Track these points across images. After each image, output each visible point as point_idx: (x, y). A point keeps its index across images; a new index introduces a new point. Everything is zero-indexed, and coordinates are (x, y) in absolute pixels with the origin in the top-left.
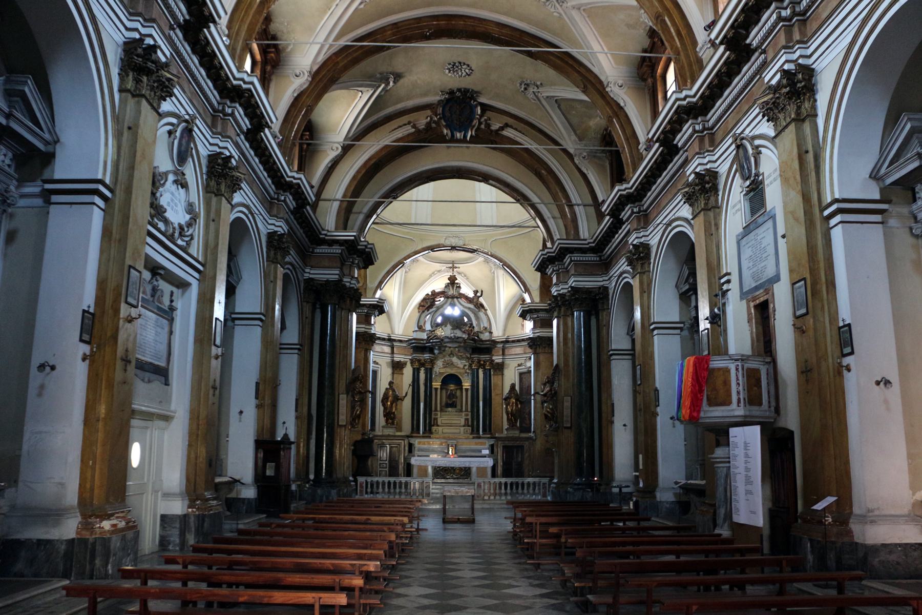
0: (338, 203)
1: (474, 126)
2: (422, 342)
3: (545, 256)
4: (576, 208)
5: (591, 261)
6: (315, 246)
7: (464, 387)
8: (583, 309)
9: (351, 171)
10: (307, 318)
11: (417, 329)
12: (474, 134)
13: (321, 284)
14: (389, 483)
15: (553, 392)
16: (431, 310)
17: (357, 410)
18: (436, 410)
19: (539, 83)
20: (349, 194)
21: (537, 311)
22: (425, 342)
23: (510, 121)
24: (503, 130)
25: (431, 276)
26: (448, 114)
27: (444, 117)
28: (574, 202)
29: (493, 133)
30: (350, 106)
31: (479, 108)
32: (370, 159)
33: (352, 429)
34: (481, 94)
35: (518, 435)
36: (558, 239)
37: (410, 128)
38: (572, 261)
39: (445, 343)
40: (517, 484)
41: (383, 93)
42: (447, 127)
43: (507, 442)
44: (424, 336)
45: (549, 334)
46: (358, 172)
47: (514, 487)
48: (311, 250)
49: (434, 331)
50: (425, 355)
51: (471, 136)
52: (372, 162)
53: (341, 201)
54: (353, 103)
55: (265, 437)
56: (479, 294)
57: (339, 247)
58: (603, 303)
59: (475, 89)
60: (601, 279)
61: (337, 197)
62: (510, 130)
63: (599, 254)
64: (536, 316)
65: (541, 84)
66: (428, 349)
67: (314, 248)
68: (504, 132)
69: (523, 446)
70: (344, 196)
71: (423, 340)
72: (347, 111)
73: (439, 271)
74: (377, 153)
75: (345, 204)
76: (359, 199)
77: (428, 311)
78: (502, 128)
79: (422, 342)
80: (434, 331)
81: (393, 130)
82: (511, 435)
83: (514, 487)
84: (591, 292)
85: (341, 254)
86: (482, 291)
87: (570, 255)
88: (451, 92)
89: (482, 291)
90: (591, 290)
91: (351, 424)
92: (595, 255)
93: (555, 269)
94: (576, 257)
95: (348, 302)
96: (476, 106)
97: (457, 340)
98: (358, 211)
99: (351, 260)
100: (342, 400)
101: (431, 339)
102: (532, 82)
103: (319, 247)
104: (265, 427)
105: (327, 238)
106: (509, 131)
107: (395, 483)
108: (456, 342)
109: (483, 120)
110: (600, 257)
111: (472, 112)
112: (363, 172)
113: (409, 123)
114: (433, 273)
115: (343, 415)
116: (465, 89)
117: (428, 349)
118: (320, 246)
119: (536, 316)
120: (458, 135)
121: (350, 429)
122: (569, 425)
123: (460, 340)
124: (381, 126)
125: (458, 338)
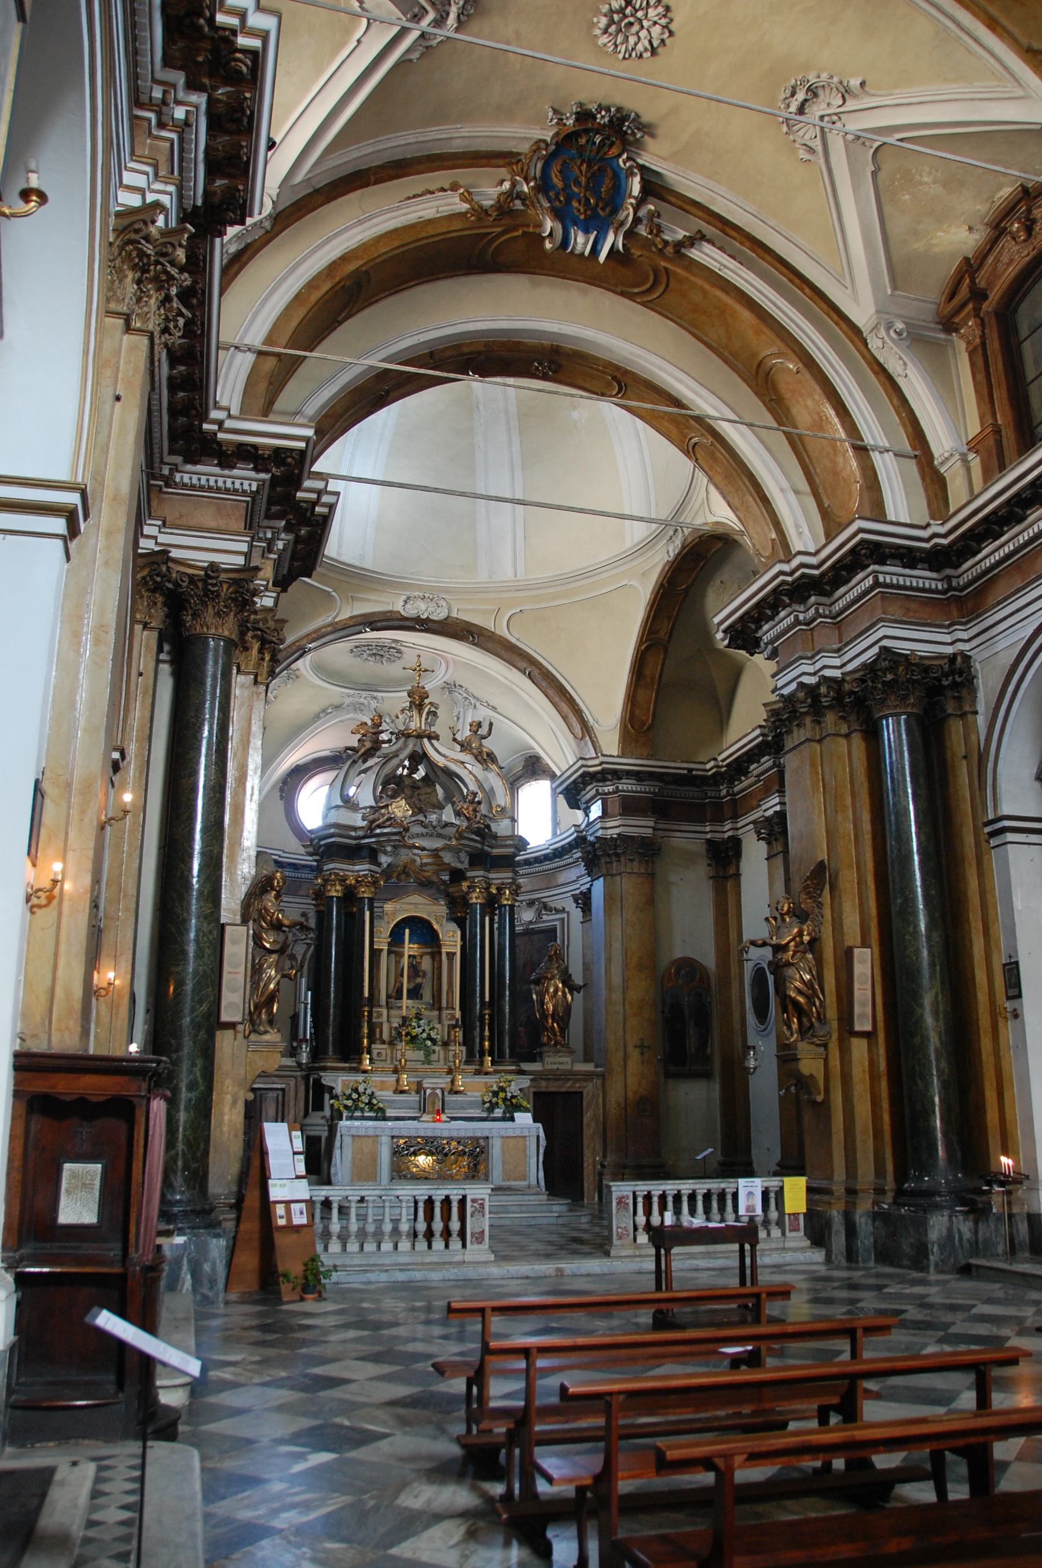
0: (250, 358)
1: (622, 224)
2: (353, 834)
3: (789, 579)
4: (875, 456)
5: (930, 591)
6: (178, 459)
7: (444, 950)
8: (909, 710)
9: (290, 281)
10: (141, 674)
11: (340, 803)
12: (620, 246)
13: (192, 578)
14: (447, 1201)
15: (806, 938)
16: (370, 762)
17: (270, 979)
18: (373, 1001)
19: (855, 83)
20: (285, 339)
21: (617, 775)
22: (361, 833)
23: (709, 230)
24: (692, 245)
25: (317, 717)
26: (557, 181)
27: (544, 186)
28: (868, 440)
29: (670, 249)
30: (319, 72)
31: (637, 179)
32: (344, 258)
33: (253, 1037)
34: (652, 136)
35: (569, 1067)
36: (800, 553)
37: (457, 200)
38: (821, 616)
39: (412, 837)
40: (722, 1196)
41: (415, 56)
42: (558, 214)
43: (543, 1084)
44: (357, 820)
45: (660, 826)
46: (311, 285)
47: (715, 1205)
48: (166, 471)
49: (386, 806)
50: (357, 868)
51: (613, 249)
52: (352, 267)
53: (260, 353)
54: (330, 63)
55: (55, 1040)
56: (483, 731)
57: (252, 474)
58: (959, 699)
59: (645, 118)
60: (948, 639)
61: (247, 341)
62: (707, 247)
63: (949, 572)
64: (611, 789)
65: (863, 84)
66: (365, 852)
67: (175, 469)
68: (693, 250)
69: (581, 1093)
70: (269, 340)
71: (355, 829)
72: (308, 89)
73: (338, 707)
74: (364, 247)
75: (270, 363)
76: (314, 354)
77: (364, 762)
78: (691, 241)
79: (353, 834)
80: (386, 806)
81: (409, 198)
82: (555, 1067)
83: (715, 1205)
84: (927, 669)
85: (254, 495)
86: (491, 724)
87: (876, 567)
88: (584, 116)
89: (491, 724)
90: (927, 662)
91: (252, 1022)
92: (934, 575)
93: (801, 617)
94: (892, 573)
95: (255, 651)
96: (630, 173)
97: (443, 832)
98: (292, 408)
99: (269, 535)
100: (234, 942)
101: (379, 826)
102: (836, 80)
103: (189, 467)
104: (59, 992)
105: (221, 436)
106: (707, 251)
107: (447, 1201)
108: (440, 836)
109: (642, 213)
110: (949, 578)
111: (618, 191)
112: (326, 287)
113: (454, 187)
114: (324, 711)
115: (234, 990)
116: (619, 109)
117: (365, 852)
118: (195, 463)
119: (611, 789)
120: (581, 239)
121: (246, 1037)
122: (868, 1028)
123: (451, 831)
124: (376, 183)
125: (447, 825)
